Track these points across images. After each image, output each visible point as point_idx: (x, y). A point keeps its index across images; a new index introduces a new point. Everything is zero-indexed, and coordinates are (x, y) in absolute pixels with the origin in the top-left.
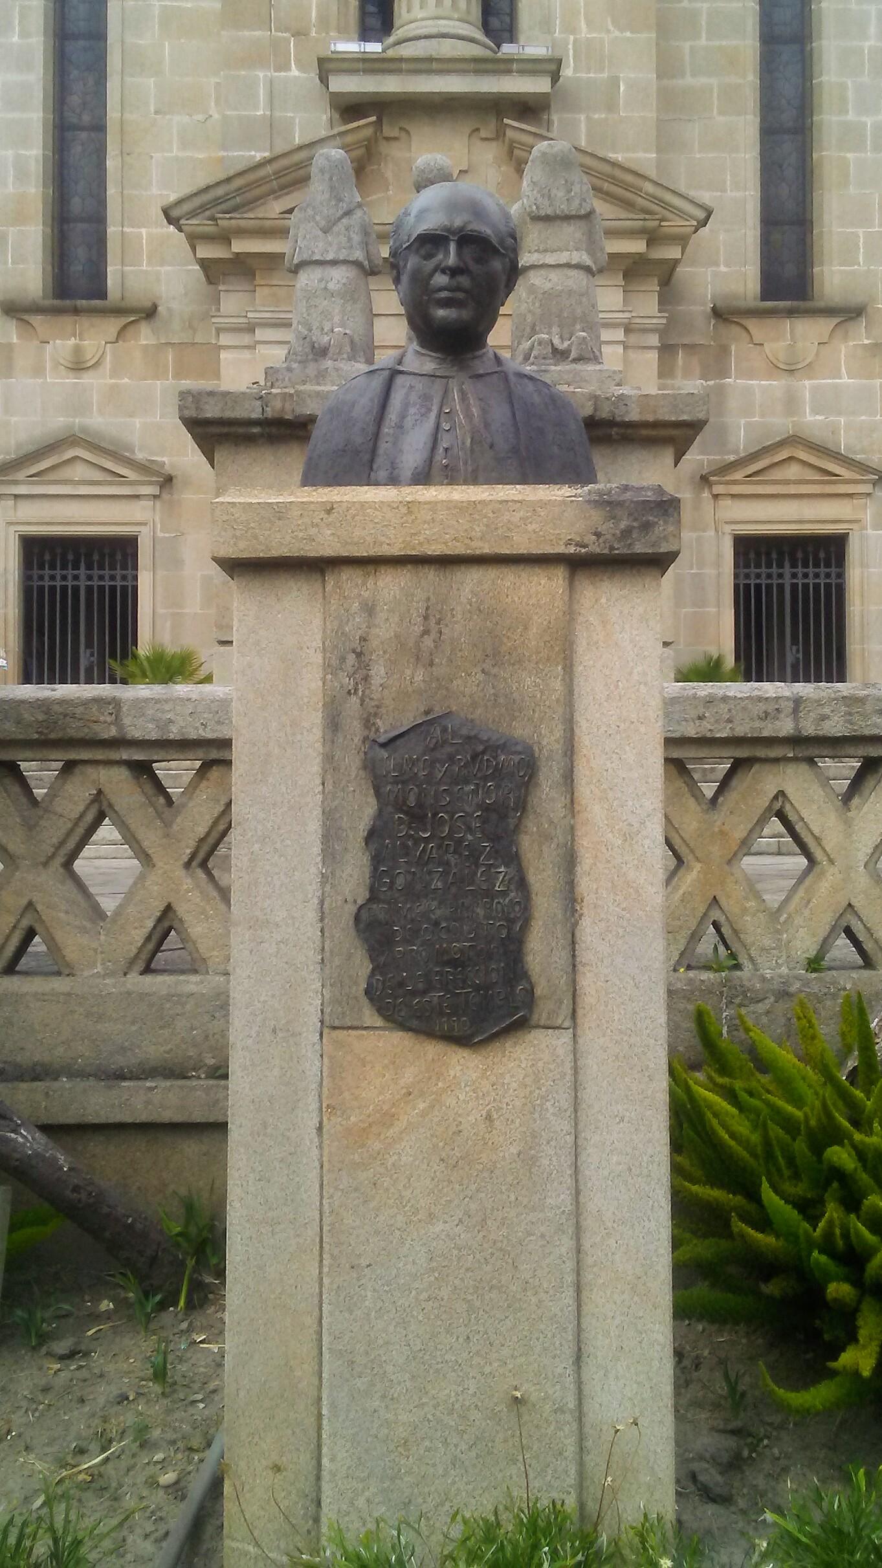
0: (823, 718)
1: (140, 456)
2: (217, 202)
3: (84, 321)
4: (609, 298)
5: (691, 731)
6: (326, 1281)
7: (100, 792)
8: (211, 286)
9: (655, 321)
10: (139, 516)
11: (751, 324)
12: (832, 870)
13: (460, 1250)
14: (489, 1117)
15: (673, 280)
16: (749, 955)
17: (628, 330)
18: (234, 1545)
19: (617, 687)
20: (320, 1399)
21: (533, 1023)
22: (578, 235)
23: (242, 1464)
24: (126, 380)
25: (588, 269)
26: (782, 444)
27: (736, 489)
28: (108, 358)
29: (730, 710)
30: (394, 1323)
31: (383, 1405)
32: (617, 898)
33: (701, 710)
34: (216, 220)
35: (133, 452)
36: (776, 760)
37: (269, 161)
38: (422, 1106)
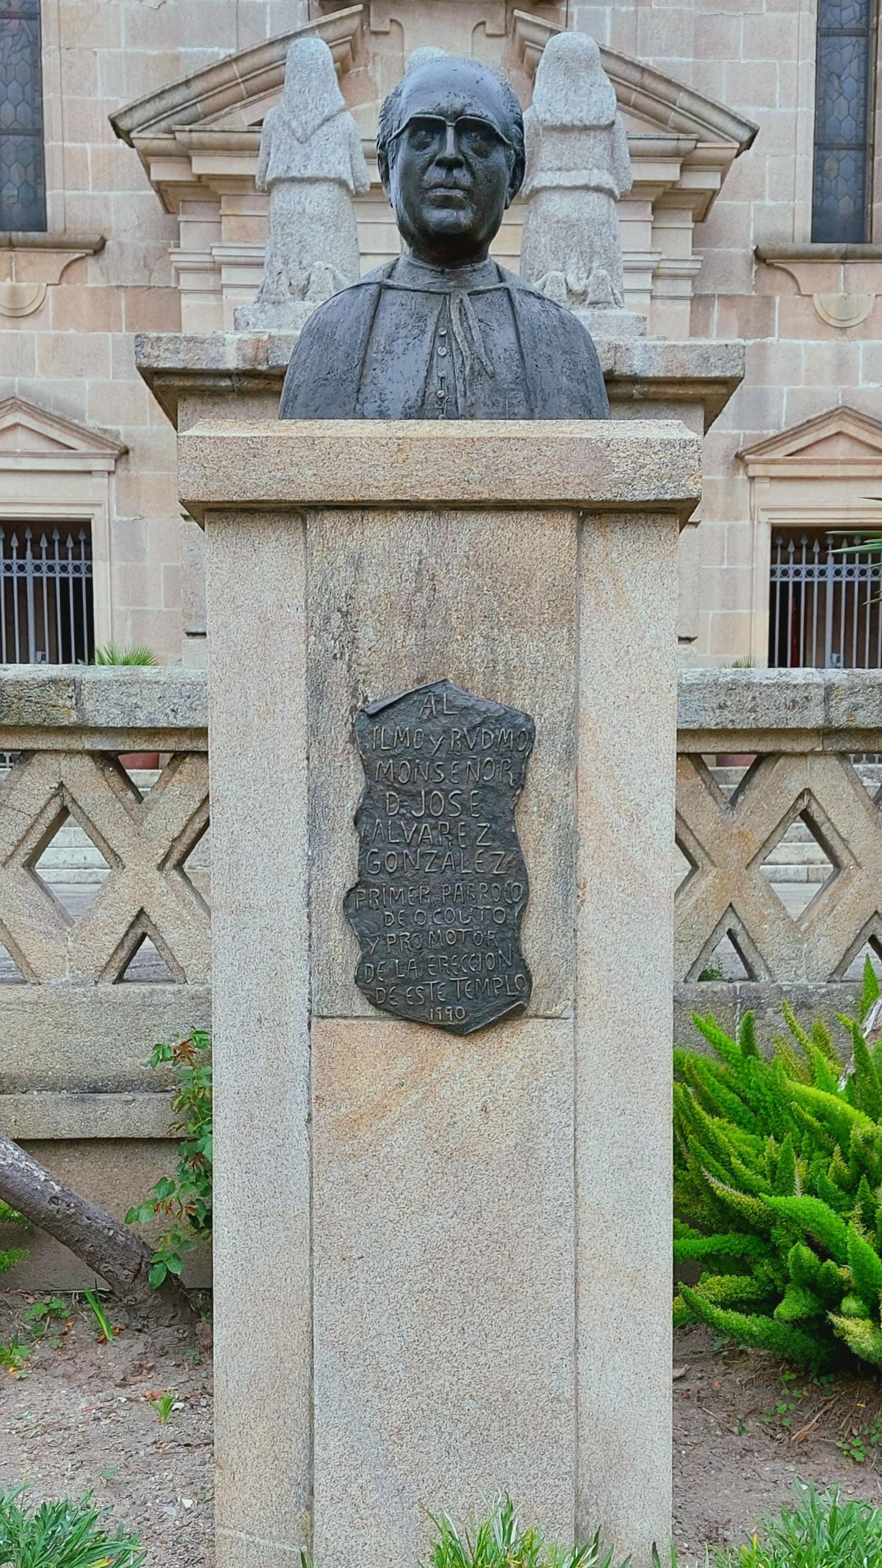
0: (856, 707)
1: (90, 423)
2: (174, 110)
3: (21, 257)
4: (634, 233)
5: (710, 721)
6: (316, 1274)
7: (61, 785)
8: (169, 216)
9: (688, 265)
10: (91, 497)
11: (799, 270)
12: (859, 874)
13: (454, 1242)
14: (485, 1109)
15: (710, 216)
16: (767, 968)
17: (655, 277)
18: (227, 1532)
19: (627, 652)
20: (311, 1389)
21: (532, 1009)
22: (599, 150)
23: (233, 1453)
24: (72, 331)
25: (610, 193)
26: (830, 415)
27: (776, 470)
28: (50, 303)
29: (754, 698)
30: (387, 1315)
31: (376, 1395)
32: (622, 883)
33: (722, 698)
34: (173, 132)
35: (82, 419)
36: (803, 755)
37: (237, 59)
38: (415, 1097)
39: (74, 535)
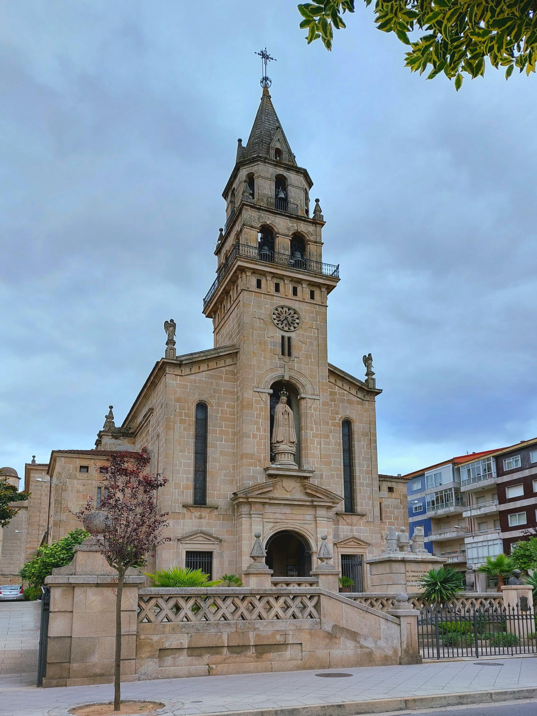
3: (202, 509)
10: (213, 548)
39: (210, 554)
